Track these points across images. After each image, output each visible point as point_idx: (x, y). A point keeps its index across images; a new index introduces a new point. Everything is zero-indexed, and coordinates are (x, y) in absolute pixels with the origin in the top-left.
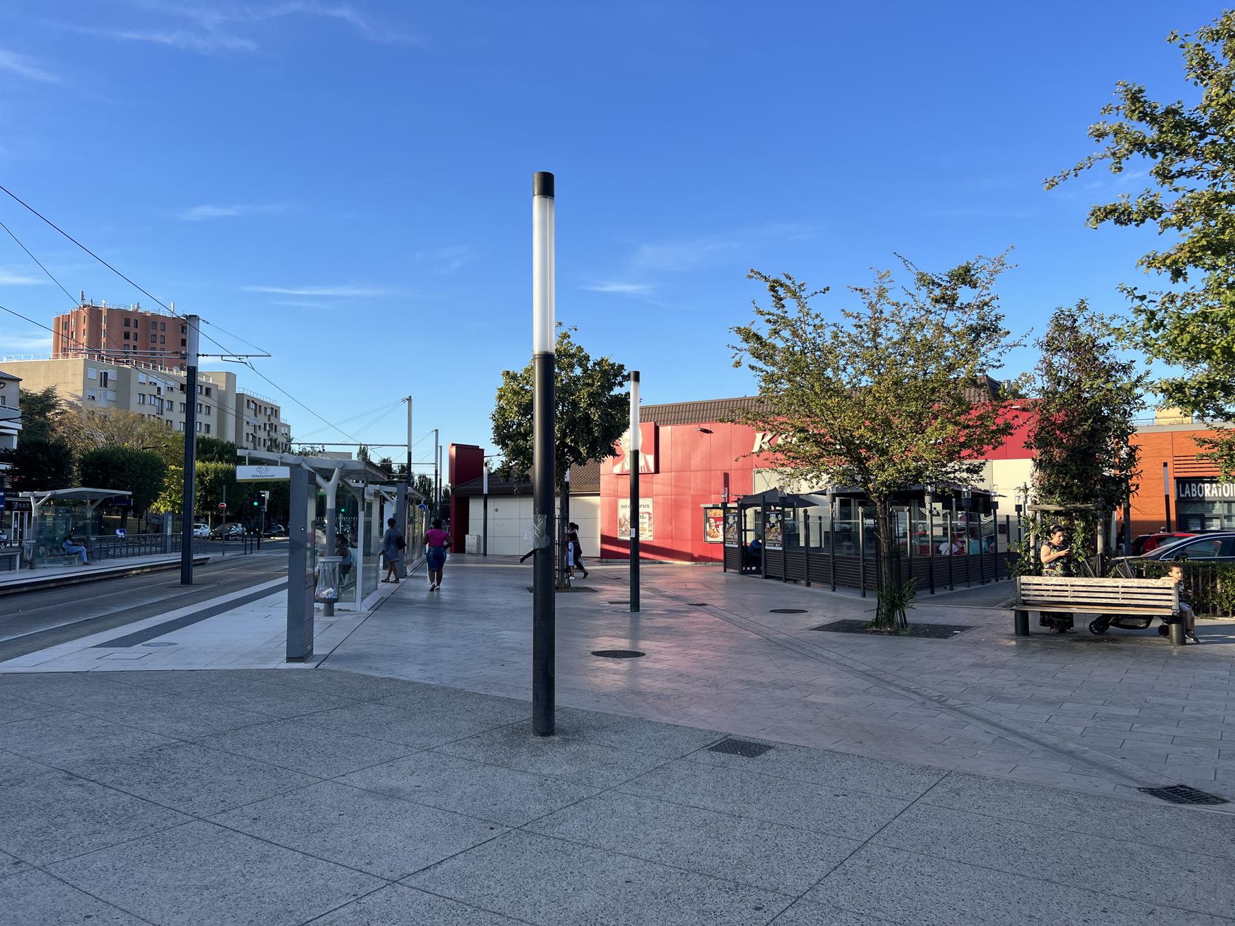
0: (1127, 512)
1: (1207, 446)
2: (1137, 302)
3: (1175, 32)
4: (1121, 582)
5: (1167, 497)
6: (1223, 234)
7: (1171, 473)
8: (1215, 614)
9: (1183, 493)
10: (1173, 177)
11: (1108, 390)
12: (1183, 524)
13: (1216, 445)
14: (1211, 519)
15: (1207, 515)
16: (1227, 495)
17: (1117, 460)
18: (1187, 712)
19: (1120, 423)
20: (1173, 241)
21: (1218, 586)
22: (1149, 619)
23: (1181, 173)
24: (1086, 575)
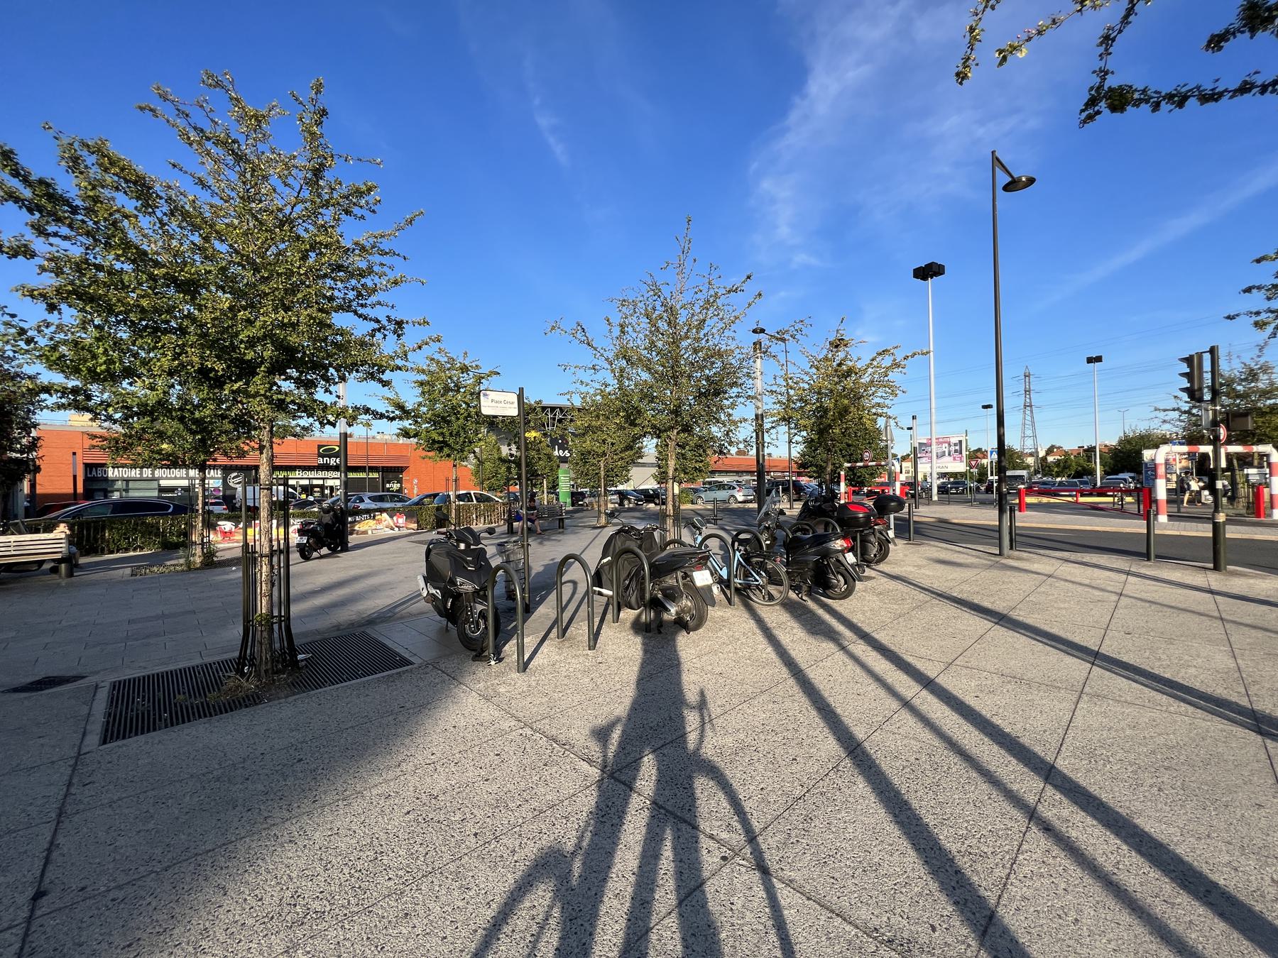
0: (33, 486)
1: (98, 440)
2: (7, 318)
3: (51, 124)
4: (13, 538)
5: (75, 477)
6: (89, 288)
7: (80, 461)
8: (103, 553)
9: (91, 473)
10: (49, 235)
11: (12, 392)
12: (88, 494)
13: (106, 440)
14: (112, 492)
15: (109, 489)
16: (125, 476)
17: (18, 446)
18: (64, 623)
19: (23, 418)
20: (49, 281)
21: (107, 535)
22: (41, 563)
23: (56, 235)
24: (20, 533)
